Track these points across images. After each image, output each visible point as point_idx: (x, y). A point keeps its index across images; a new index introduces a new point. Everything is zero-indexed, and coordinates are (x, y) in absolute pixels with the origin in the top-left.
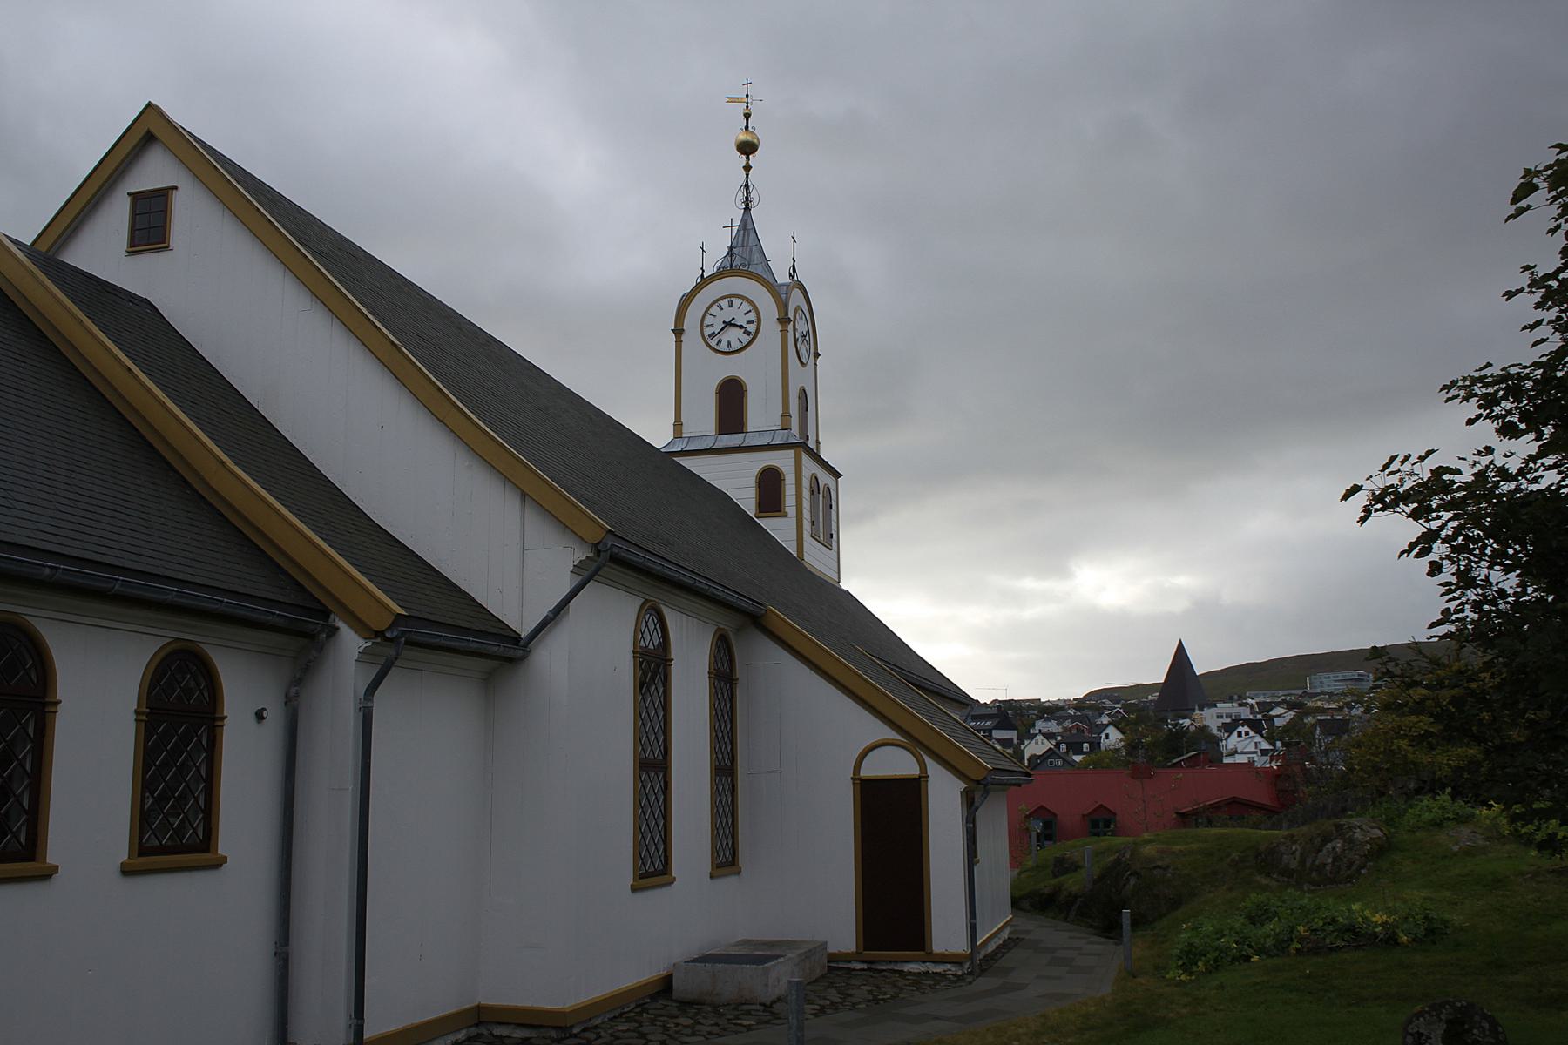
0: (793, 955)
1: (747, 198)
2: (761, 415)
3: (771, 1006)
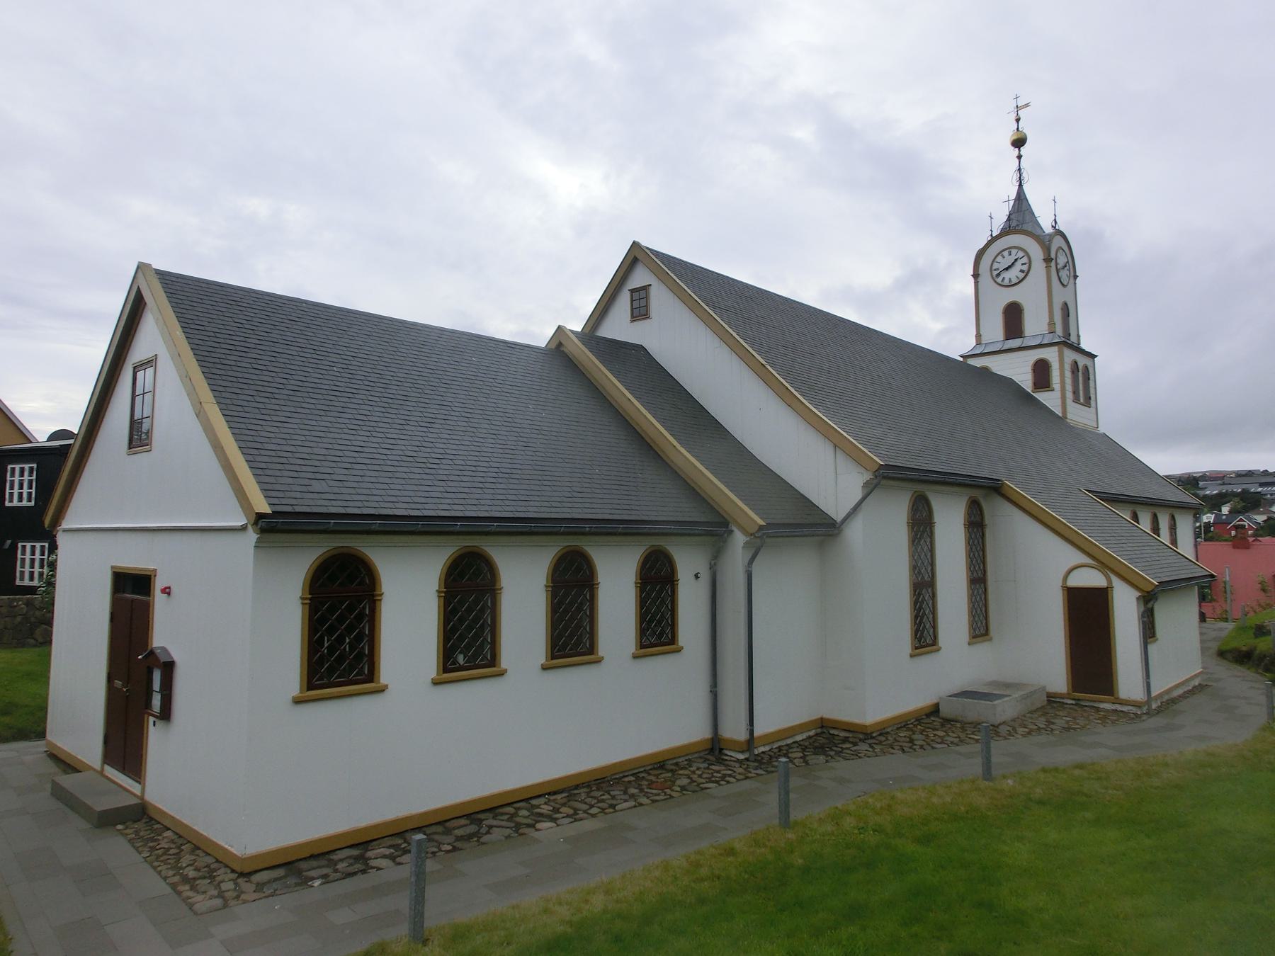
0: (1017, 694)
1: (1020, 178)
2: (1035, 325)
3: (997, 727)
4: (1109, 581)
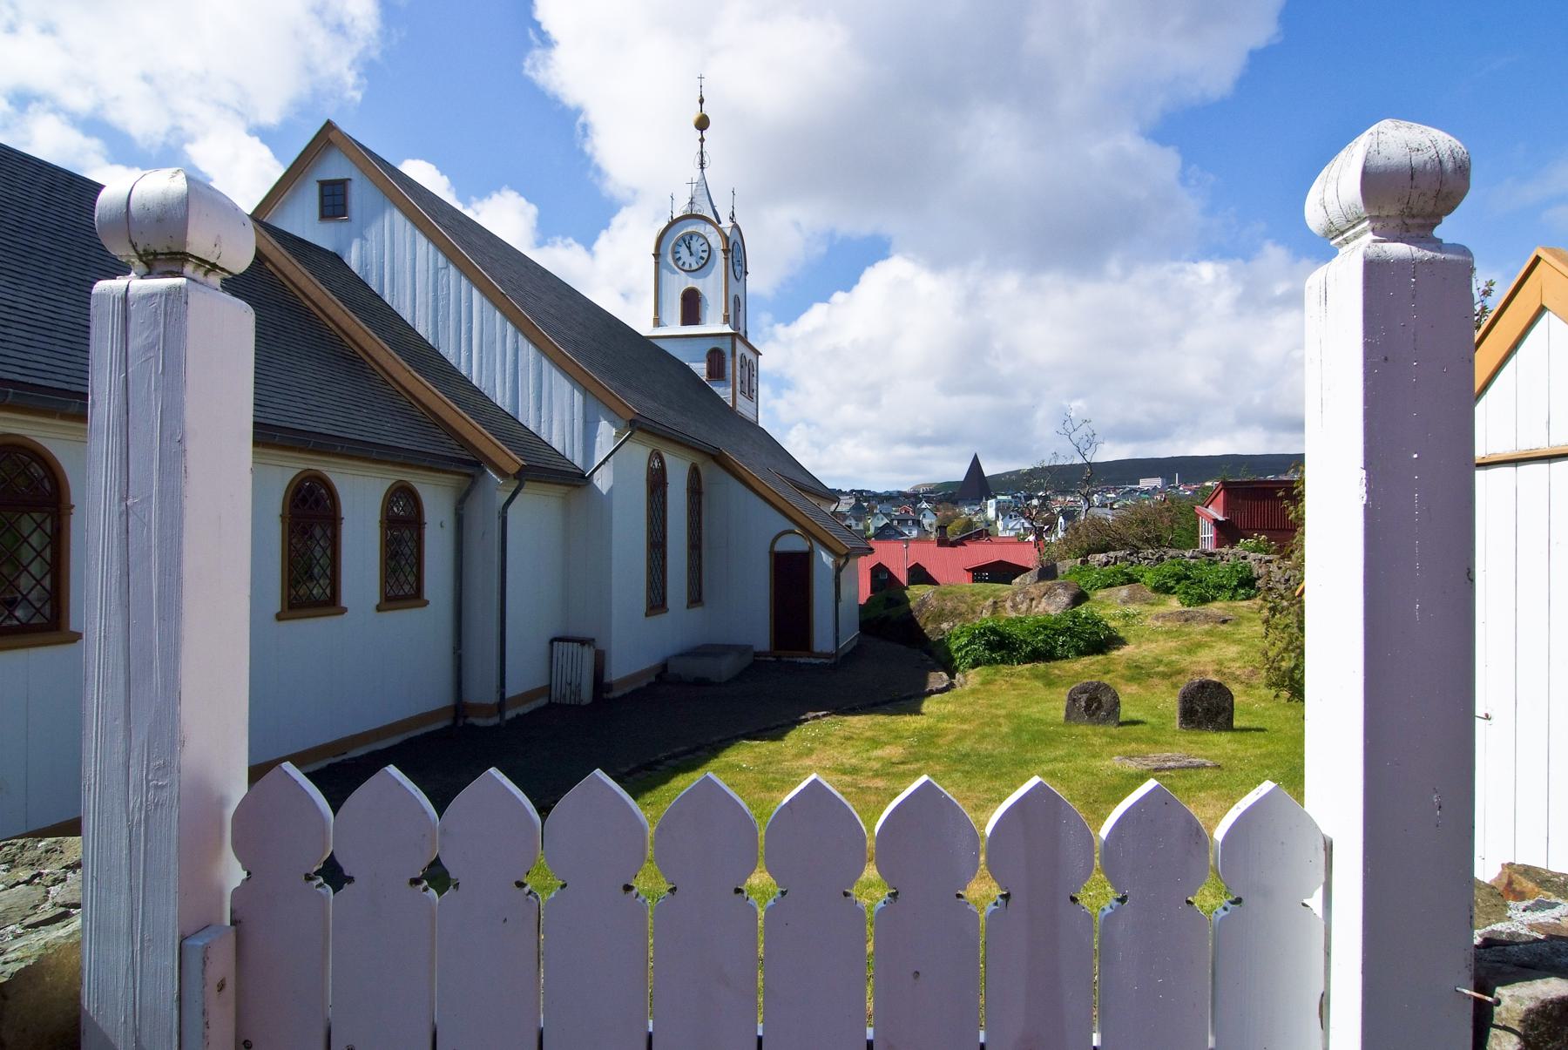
4: (811, 548)
